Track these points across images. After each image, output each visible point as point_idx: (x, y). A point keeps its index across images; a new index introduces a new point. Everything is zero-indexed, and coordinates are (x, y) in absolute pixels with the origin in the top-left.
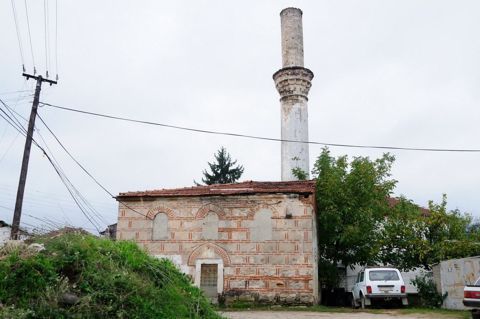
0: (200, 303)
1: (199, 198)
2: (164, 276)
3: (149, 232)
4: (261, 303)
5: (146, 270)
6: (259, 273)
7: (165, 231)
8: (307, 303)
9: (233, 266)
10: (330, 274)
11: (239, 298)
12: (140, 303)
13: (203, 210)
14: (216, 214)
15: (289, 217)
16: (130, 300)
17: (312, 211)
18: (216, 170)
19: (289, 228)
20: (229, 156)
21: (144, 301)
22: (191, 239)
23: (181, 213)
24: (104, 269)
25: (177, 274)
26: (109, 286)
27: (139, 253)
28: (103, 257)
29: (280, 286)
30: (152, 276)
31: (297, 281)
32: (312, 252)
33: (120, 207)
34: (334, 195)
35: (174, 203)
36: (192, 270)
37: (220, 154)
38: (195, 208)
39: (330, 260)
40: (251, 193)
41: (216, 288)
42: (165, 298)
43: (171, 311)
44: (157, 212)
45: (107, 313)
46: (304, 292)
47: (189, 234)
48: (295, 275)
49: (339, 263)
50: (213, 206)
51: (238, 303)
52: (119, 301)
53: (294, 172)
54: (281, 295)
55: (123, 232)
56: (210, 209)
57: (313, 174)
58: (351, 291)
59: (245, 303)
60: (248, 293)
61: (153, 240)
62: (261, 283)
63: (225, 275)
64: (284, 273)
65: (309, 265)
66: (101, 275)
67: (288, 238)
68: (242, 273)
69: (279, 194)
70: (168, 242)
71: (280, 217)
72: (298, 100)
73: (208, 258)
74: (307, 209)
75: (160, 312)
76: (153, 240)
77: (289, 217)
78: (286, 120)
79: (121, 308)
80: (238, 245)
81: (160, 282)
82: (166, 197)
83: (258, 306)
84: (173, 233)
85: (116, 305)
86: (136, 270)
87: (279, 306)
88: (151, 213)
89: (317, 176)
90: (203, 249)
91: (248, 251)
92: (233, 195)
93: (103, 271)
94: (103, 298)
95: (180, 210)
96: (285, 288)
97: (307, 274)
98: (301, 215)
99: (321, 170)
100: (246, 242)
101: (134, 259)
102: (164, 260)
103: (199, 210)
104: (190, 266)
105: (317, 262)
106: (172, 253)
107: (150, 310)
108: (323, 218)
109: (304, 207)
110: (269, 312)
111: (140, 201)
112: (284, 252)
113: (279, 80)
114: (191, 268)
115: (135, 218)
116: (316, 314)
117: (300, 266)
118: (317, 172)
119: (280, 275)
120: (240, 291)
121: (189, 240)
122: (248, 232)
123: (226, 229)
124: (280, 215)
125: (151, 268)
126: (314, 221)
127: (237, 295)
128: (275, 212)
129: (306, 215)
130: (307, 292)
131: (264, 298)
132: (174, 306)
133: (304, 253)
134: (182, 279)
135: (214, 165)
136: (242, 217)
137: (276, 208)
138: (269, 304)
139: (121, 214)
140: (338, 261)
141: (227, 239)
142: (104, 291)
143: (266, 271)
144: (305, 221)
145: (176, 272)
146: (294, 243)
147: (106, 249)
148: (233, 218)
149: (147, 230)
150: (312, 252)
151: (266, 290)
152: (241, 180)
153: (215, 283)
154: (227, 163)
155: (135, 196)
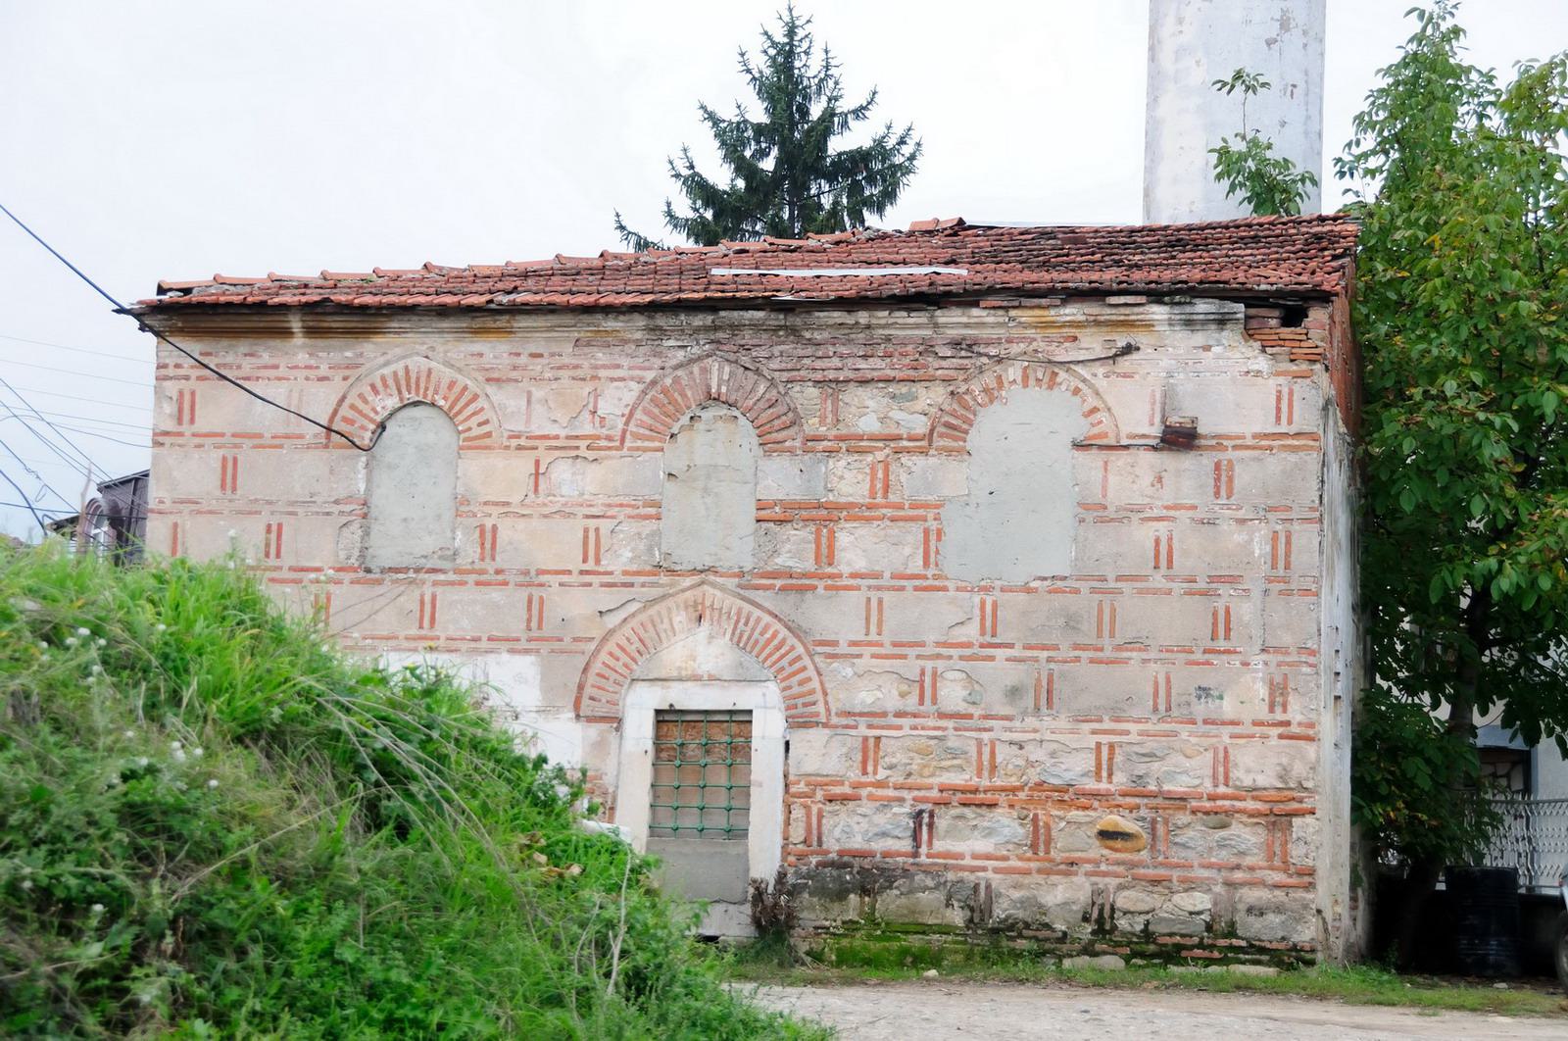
0: (631, 929)
1: (640, 321)
2: (417, 769)
3: (344, 520)
4: (1004, 943)
5: (308, 736)
6: (993, 768)
7: (439, 517)
8: (1282, 946)
9: (844, 721)
10: (1425, 783)
11: (873, 908)
12: (273, 923)
13: (665, 391)
14: (742, 420)
15: (1179, 438)
16: (211, 906)
17: (1325, 408)
18: (748, 153)
19: (1176, 507)
20: (827, 68)
21: (300, 912)
22: (598, 561)
23: (538, 409)
24: (57, 729)
25: (498, 762)
26: (80, 822)
27: (272, 635)
28: (45, 658)
29: (1119, 844)
30: (346, 772)
31: (1219, 818)
32: (1313, 653)
33: (163, 372)
34: (1469, 312)
35: (493, 351)
36: (600, 746)
37: (772, 52)
38: (618, 378)
39: (1426, 698)
40: (958, 295)
41: (740, 850)
42: (426, 896)
43: (456, 969)
44: (393, 402)
45: (68, 982)
46: (1263, 884)
47: (586, 538)
48: (1208, 786)
49: (1489, 723)
50: (727, 369)
51: (870, 937)
52: (143, 913)
53: (1228, 163)
54: (1123, 901)
55: (188, 523)
56: (709, 387)
57: (1342, 174)
58: (1555, 892)
59: (911, 938)
60: (930, 883)
61: (368, 571)
62: (1007, 825)
63: (791, 778)
64: (1141, 769)
65: (1294, 729)
66: (34, 763)
67: (1170, 565)
68: (891, 767)
69: (1122, 300)
70: (462, 583)
71: (1124, 442)
73: (696, 678)
74: (1291, 393)
75: (393, 975)
76: (368, 571)
77: (1179, 438)
79: (160, 953)
80: (874, 604)
81: (394, 803)
82: (443, 312)
83: (984, 957)
84: (489, 526)
85: (125, 939)
86: (249, 733)
87: (1112, 962)
88: (353, 407)
89: (1370, 190)
90: (666, 625)
91: (931, 638)
92: (844, 303)
93: (44, 742)
94: (44, 896)
95: (529, 394)
96: (1144, 855)
97: (1281, 777)
98: (1258, 429)
99: (1395, 155)
100: (918, 583)
101: (241, 670)
102: (419, 678)
103: (644, 392)
104: (591, 719)
105: (1346, 709)
106: (484, 644)
107: (337, 962)
108: (1394, 457)
109: (1272, 382)
110: (1053, 996)
111: (287, 333)
112: (1146, 648)
114: (594, 730)
115: (260, 436)
116: (1333, 1013)
117: (1237, 730)
118: (1373, 162)
119: (1120, 780)
120: (883, 870)
121: (582, 572)
122: (933, 525)
123: (801, 506)
124: (1125, 430)
125: (344, 722)
126: (1335, 466)
127: (865, 891)
128: (1094, 410)
129: (1283, 428)
130: (1277, 886)
131: (1020, 914)
132: (476, 944)
133: (1264, 657)
134: (529, 791)
135: (741, 126)
136: (899, 438)
137: (1101, 383)
138: (1047, 946)
139: (169, 408)
140: (1484, 712)
141: (809, 565)
142: (54, 857)
143: (1036, 753)
144: (1276, 464)
145: (494, 751)
146: (1204, 593)
147: (65, 611)
148: (843, 445)
149: (335, 509)
150: (1313, 653)
151: (1033, 865)
152: (895, 219)
153: (737, 822)
154: (816, 110)
155: (254, 304)
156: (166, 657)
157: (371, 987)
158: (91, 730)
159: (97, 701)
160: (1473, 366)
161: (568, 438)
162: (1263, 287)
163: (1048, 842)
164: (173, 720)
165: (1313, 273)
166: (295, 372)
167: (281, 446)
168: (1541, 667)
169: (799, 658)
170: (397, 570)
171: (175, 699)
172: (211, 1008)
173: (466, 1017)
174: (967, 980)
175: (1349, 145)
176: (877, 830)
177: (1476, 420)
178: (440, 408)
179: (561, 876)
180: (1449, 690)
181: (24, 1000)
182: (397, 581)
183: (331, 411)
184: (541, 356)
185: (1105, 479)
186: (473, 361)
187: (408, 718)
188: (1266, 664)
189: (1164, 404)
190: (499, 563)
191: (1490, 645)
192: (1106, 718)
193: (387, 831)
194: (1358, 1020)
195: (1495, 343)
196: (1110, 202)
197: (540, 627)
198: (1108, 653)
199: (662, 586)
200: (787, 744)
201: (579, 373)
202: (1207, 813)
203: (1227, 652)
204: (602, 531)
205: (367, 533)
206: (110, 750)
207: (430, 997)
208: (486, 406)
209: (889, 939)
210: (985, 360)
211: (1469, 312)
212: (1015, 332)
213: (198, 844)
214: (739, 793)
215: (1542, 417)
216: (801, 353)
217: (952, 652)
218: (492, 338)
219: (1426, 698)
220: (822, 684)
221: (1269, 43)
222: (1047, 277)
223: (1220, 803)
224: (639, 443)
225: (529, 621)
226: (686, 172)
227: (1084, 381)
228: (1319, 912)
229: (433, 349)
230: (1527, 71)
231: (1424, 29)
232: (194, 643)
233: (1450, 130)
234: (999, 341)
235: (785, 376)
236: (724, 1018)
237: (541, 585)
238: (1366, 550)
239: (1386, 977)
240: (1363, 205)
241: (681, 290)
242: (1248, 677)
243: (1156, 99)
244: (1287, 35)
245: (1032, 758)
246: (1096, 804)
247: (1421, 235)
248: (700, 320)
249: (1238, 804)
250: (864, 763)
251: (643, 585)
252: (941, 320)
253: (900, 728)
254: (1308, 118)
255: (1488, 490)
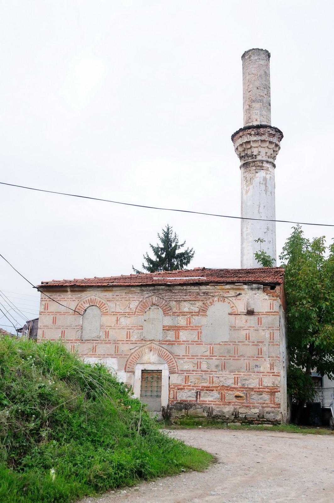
0: (142, 420)
1: (139, 288)
2: (97, 385)
4: (215, 420)
5: (75, 378)
6: (213, 382)
7: (97, 329)
8: (274, 420)
9: (181, 372)
10: (302, 385)
11: (188, 413)
13: (144, 303)
15: (250, 313)
16: (56, 415)
17: (280, 307)
18: (159, 254)
21: (74, 417)
22: (130, 338)
23: (117, 306)
24: (25, 377)
28: (23, 362)
29: (239, 398)
30: (83, 386)
31: (260, 393)
32: (279, 358)
33: (42, 299)
34: (307, 287)
35: (109, 295)
36: (130, 378)
38: (134, 300)
40: (204, 283)
44: (88, 305)
45: (28, 432)
46: (269, 407)
47: (127, 333)
48: (258, 386)
49: (314, 371)
51: (187, 419)
53: (258, 256)
54: (241, 411)
57: (281, 259)
58: (329, 408)
59: (196, 419)
60: (200, 407)
61: (82, 340)
62: (216, 395)
63: (170, 384)
65: (275, 374)
67: (249, 339)
68: (191, 382)
69: (238, 284)
72: (263, 167)
73: (150, 363)
74: (273, 304)
75: (93, 430)
77: (250, 313)
78: (247, 192)
81: (93, 393)
82: (99, 287)
83: (211, 423)
84: (107, 331)
86: (63, 378)
87: (238, 424)
88: (80, 306)
89: (286, 262)
90: (144, 352)
94: (23, 413)
96: (245, 401)
98: (266, 311)
100: (196, 343)
101: (61, 365)
103: (139, 303)
104: (128, 372)
105: (285, 369)
106: (106, 356)
107: (81, 428)
109: (269, 301)
111: (67, 291)
112: (244, 357)
113: (240, 141)
114: (129, 374)
115: (61, 312)
117: (264, 374)
118: (287, 257)
119: (240, 385)
120: (190, 404)
121: (126, 341)
122: (200, 331)
125: (82, 376)
126: (282, 318)
127: (186, 409)
128: (233, 307)
130: (272, 407)
132: (110, 423)
133: (269, 358)
134: (120, 390)
135: (158, 248)
136: (192, 312)
137: (234, 301)
139: (43, 307)
140: (313, 369)
141: (174, 339)
143: (222, 379)
144: (270, 318)
147: (27, 352)
148: (181, 314)
150: (279, 358)
151: (221, 403)
152: (190, 267)
153: (159, 394)
154: (173, 245)
156: (46, 362)
157: (89, 433)
158: (32, 377)
159: (33, 371)
160: (309, 298)
161: (124, 312)
162: (267, 282)
163: (224, 398)
164: (48, 375)
165: (276, 279)
166: (68, 299)
167: (65, 315)
168: (324, 360)
169: (172, 359)
170: (88, 340)
171: (48, 371)
172: (56, 437)
173: (108, 439)
174: (208, 428)
175: (282, 253)
176: (188, 396)
177: (310, 309)
178: (98, 306)
179: (127, 408)
180: (306, 365)
181: (19, 436)
182: (88, 343)
183: (75, 307)
184: (118, 296)
185: (235, 321)
186: (105, 297)
187: (95, 374)
188: (269, 360)
189: (247, 306)
190: (110, 338)
191: (313, 355)
192: (236, 372)
193: (91, 399)
194: (291, 436)
195: (313, 293)
196: (235, 265)
197: (118, 352)
198: (236, 358)
199: (143, 343)
200: (169, 377)
201: (126, 299)
202: (258, 392)
203: (261, 357)
204: (131, 332)
205: (82, 333)
206: (36, 382)
207: (101, 435)
208: (107, 306)
209: (191, 419)
210: (210, 296)
211: (307, 287)
212: (216, 291)
213: (53, 402)
214: (160, 387)
215: (323, 308)
216: (172, 295)
217: (204, 357)
218: (108, 292)
219: (301, 367)
220: (177, 364)
221: (265, 233)
222: (223, 279)
223: (260, 390)
224: (138, 314)
225: (115, 351)
226: (147, 257)
227: (231, 301)
228: (281, 413)
229: (96, 294)
230: (315, 239)
231: (295, 231)
232: (52, 359)
233: (301, 250)
234: (213, 293)
235: (169, 300)
236: (162, 440)
237: (118, 343)
238: (288, 336)
239: (295, 427)
240: (285, 265)
241: (147, 282)
242: (266, 363)
243: (243, 243)
244: (268, 232)
245: (221, 380)
246: (234, 390)
247: (297, 271)
248: (151, 288)
249: (264, 390)
250: (186, 381)
251: (139, 343)
252: (201, 288)
253: (193, 374)
254: (273, 247)
255: (313, 323)
